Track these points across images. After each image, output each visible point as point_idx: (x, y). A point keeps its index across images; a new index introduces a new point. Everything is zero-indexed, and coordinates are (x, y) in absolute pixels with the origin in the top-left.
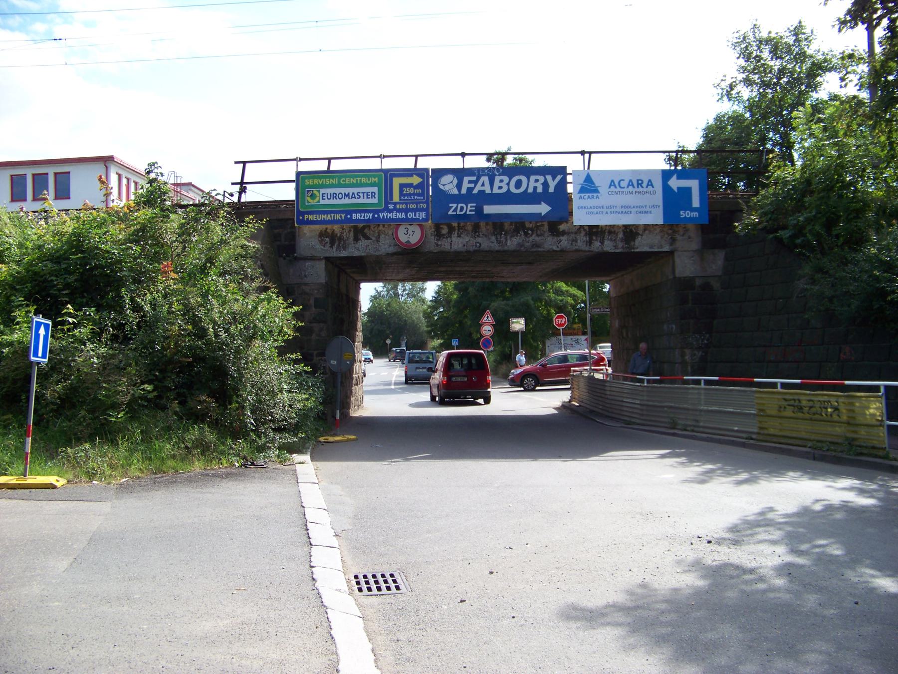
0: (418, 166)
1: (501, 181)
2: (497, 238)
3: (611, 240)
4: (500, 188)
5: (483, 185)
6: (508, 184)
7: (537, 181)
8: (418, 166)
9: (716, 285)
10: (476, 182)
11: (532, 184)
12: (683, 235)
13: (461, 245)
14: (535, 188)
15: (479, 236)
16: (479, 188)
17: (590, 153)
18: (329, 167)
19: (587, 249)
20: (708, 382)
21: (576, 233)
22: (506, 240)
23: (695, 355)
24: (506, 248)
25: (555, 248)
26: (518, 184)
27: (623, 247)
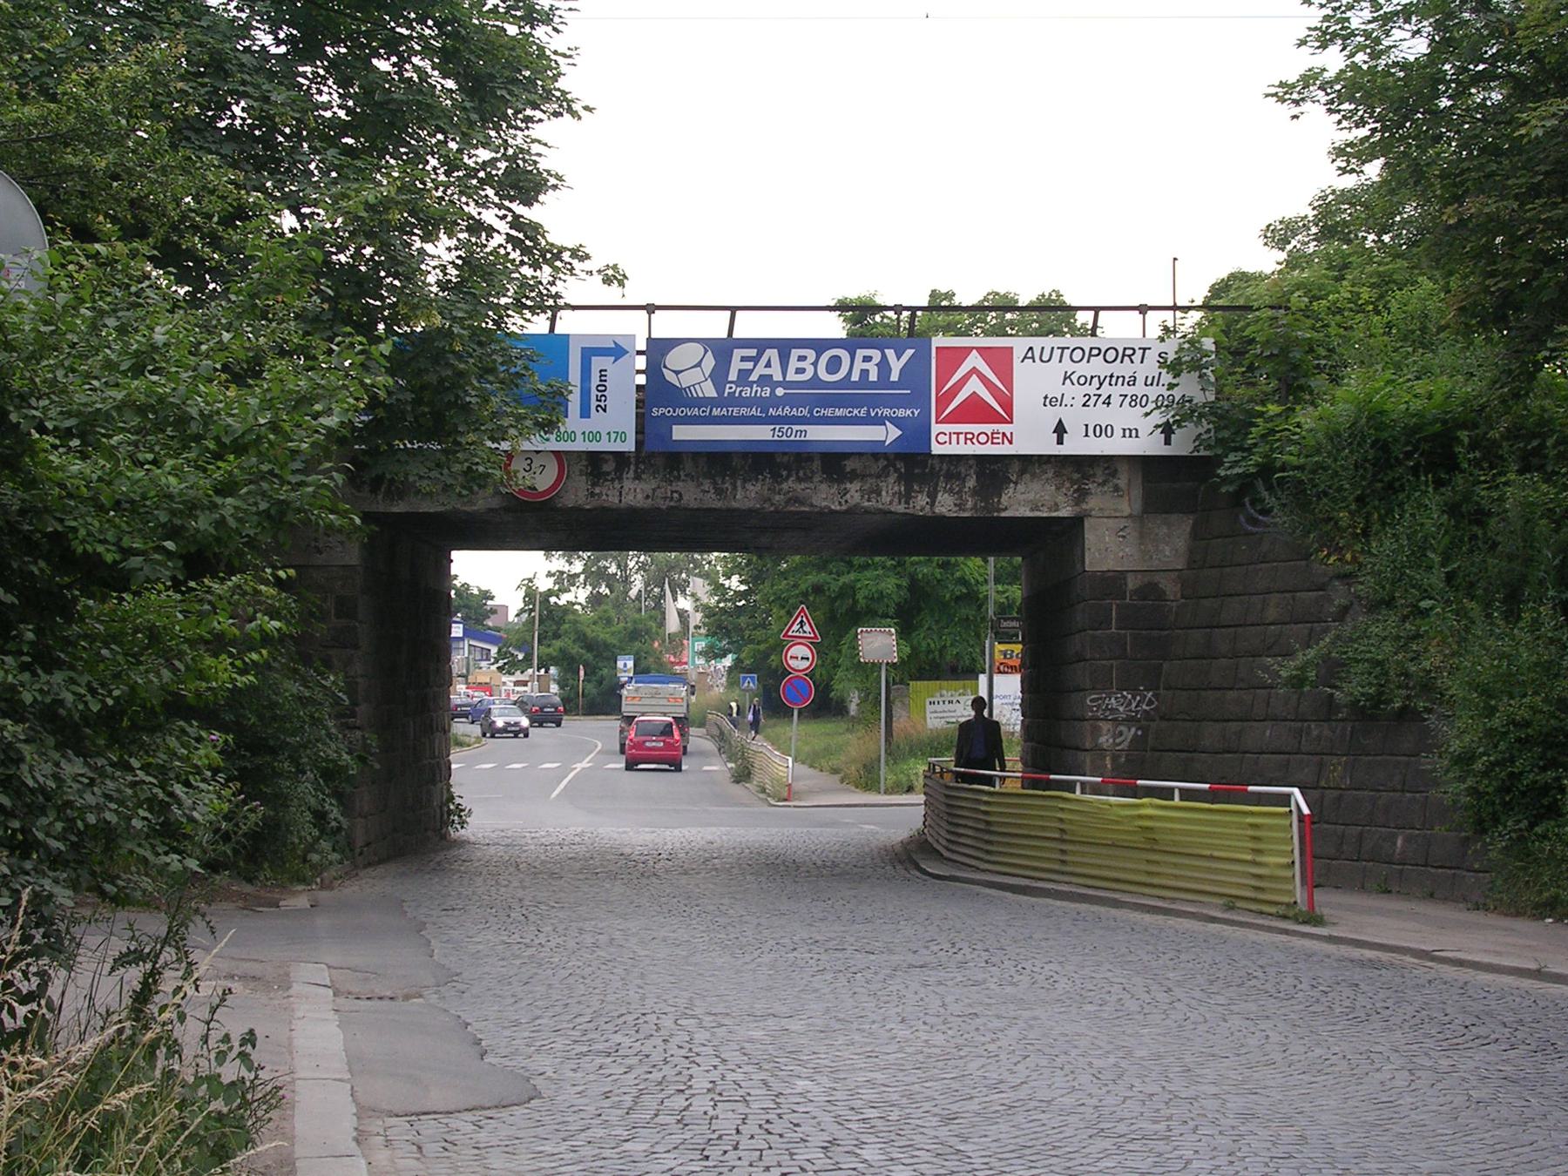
0: (735, 336)
1: (802, 358)
2: (715, 483)
3: (951, 491)
4: (800, 371)
5: (768, 365)
6: (815, 364)
7: (867, 359)
8: (735, 336)
9: (1170, 588)
10: (756, 360)
11: (859, 365)
12: (1103, 484)
13: (640, 496)
14: (865, 373)
15: (678, 478)
16: (760, 370)
18: (552, 328)
19: (901, 508)
20: (1187, 795)
21: (878, 477)
22: (735, 488)
23: (1121, 734)
24: (735, 505)
27: (974, 508)
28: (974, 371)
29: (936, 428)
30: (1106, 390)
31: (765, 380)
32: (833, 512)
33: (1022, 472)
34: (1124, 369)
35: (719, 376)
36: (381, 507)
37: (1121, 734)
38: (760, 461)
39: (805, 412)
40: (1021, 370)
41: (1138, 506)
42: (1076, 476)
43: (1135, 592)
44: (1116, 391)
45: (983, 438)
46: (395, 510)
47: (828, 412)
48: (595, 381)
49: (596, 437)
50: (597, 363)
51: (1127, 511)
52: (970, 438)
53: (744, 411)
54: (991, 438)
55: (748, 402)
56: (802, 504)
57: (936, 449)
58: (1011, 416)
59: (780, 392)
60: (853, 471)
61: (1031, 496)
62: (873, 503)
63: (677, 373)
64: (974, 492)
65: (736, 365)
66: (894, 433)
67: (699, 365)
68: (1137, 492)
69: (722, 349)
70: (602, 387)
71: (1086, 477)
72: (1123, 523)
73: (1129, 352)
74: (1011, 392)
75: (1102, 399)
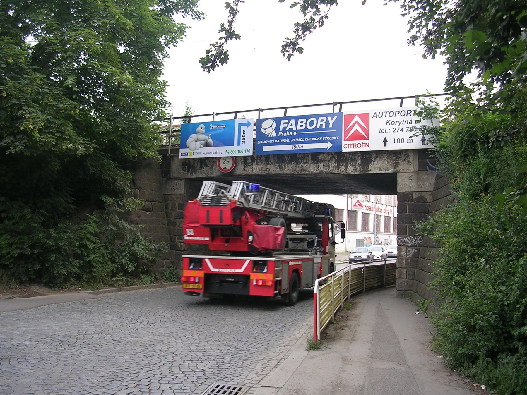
0: (287, 115)
1: (302, 122)
2: (279, 165)
3: (352, 164)
4: (301, 126)
5: (292, 125)
6: (306, 123)
7: (322, 121)
8: (287, 115)
9: (429, 198)
10: (288, 123)
12: (404, 160)
13: (258, 170)
14: (321, 125)
17: (341, 104)
19: (336, 171)
21: (329, 161)
22: (285, 166)
23: (409, 251)
24: (285, 172)
25: (315, 172)
26: (312, 123)
27: (360, 170)
28: (357, 122)
29: (344, 143)
30: (401, 126)
31: (291, 130)
32: (315, 174)
33: (376, 157)
34: (406, 118)
35: (277, 130)
36: (190, 176)
37: (409, 251)
38: (294, 157)
39: (303, 140)
40: (372, 121)
41: (416, 168)
42: (395, 158)
43: (416, 199)
44: (405, 126)
45: (359, 145)
46: (193, 177)
47: (310, 139)
48: (242, 134)
49: (241, 151)
50: (243, 128)
51: (412, 170)
52: (355, 146)
53: (284, 140)
54: (362, 145)
55: (285, 137)
56: (306, 171)
57: (344, 150)
58: (368, 136)
59: (295, 133)
60: (321, 159)
61: (379, 166)
62: (327, 170)
63: (265, 129)
64: (360, 165)
65: (282, 126)
66: (330, 145)
67: (271, 126)
68: (416, 163)
69: (277, 121)
70: (244, 136)
71: (398, 158)
72: (411, 174)
73: (409, 112)
74: (369, 129)
75: (400, 129)
